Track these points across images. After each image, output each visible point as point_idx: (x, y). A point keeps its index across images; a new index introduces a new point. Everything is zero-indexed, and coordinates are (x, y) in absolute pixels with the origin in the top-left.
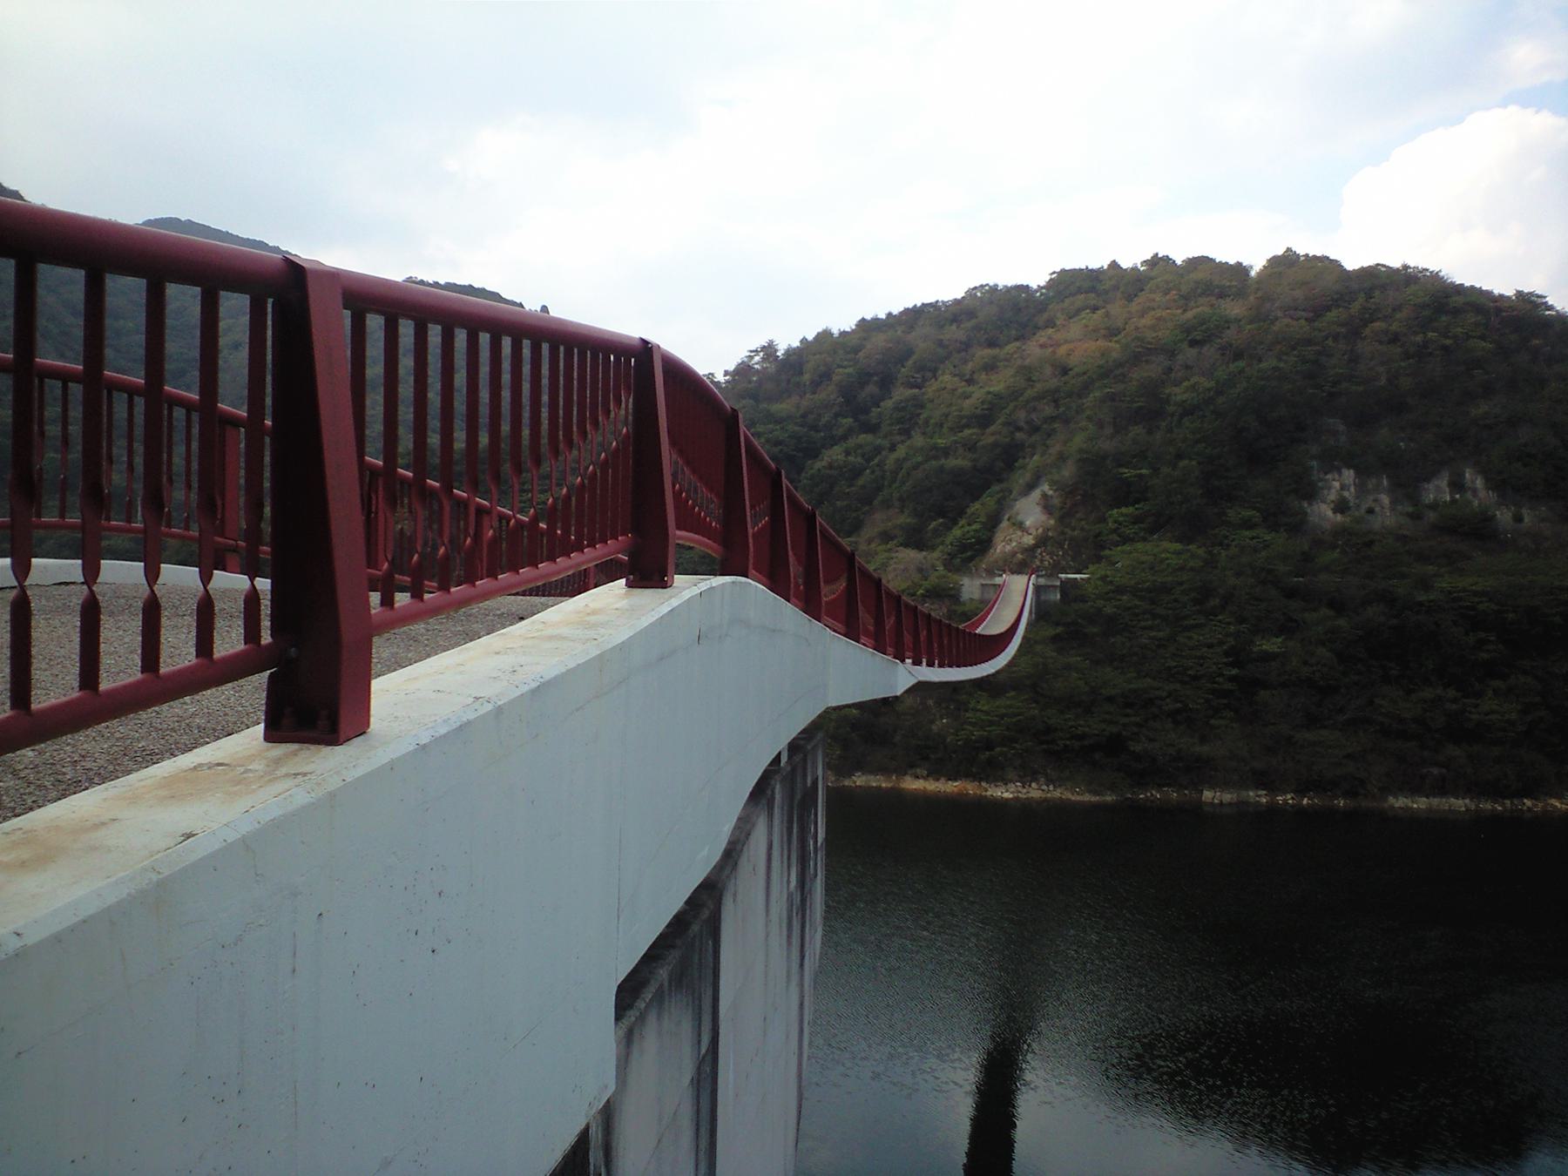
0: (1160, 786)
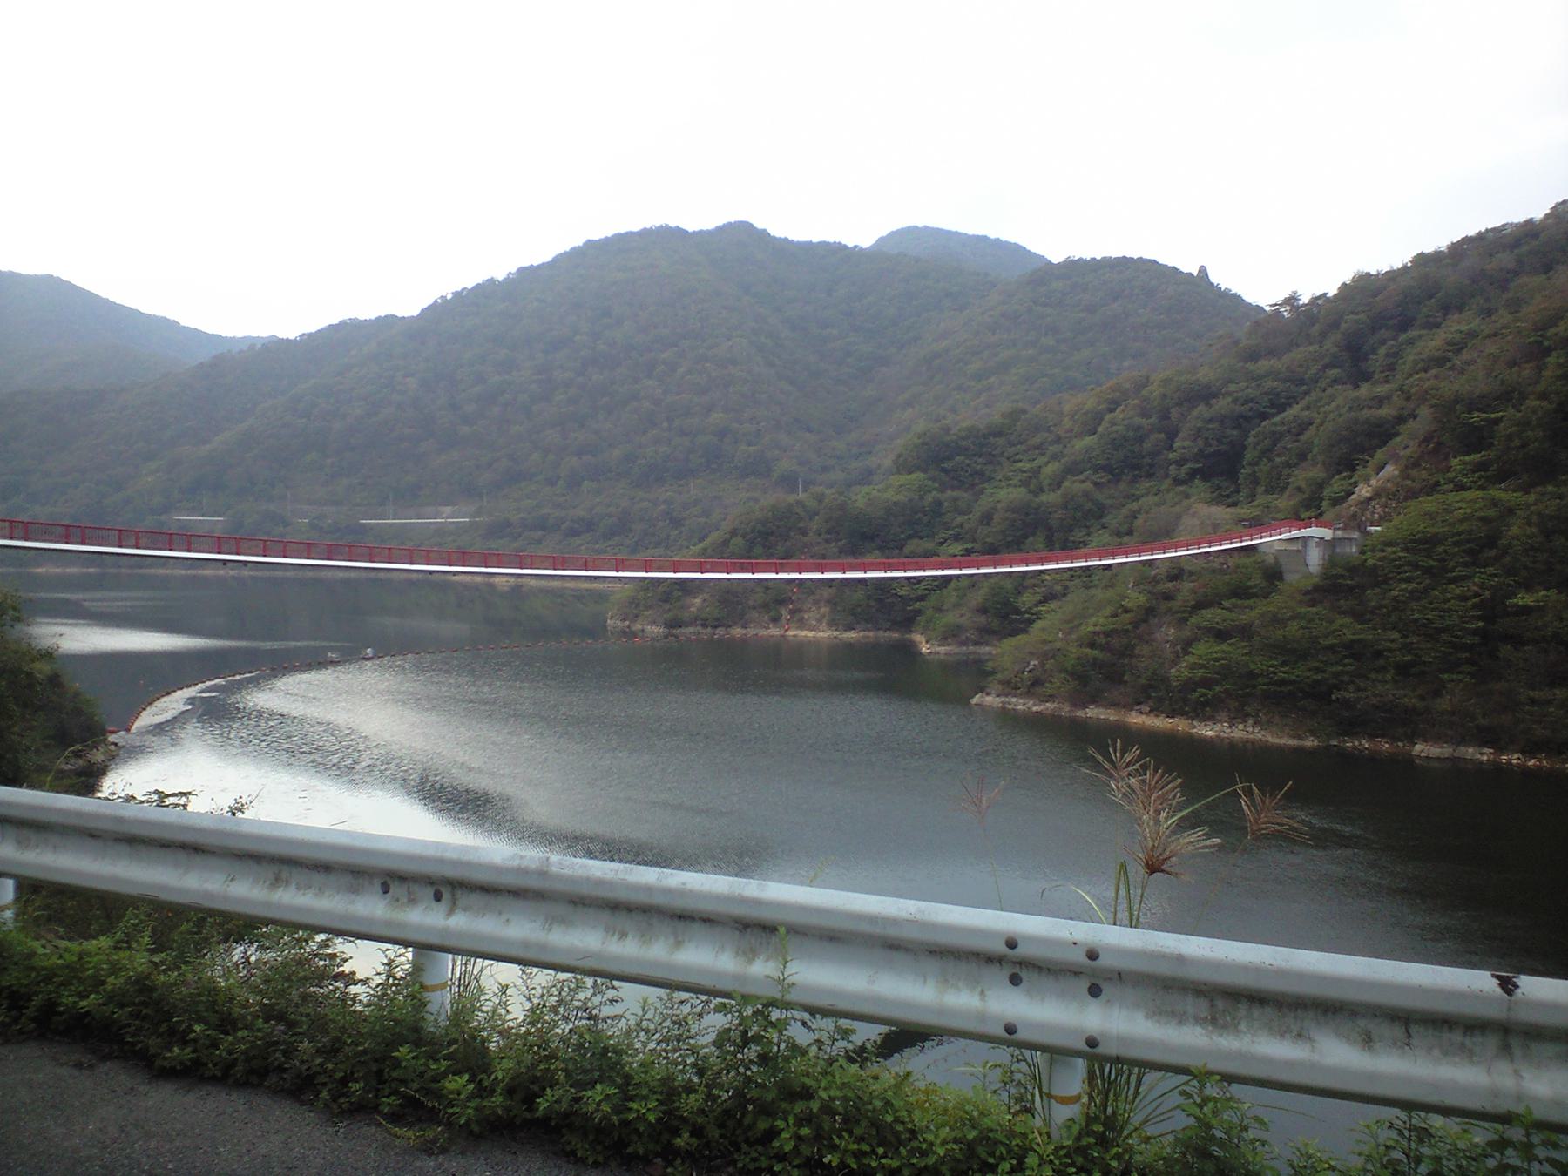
0: (1372, 737)
